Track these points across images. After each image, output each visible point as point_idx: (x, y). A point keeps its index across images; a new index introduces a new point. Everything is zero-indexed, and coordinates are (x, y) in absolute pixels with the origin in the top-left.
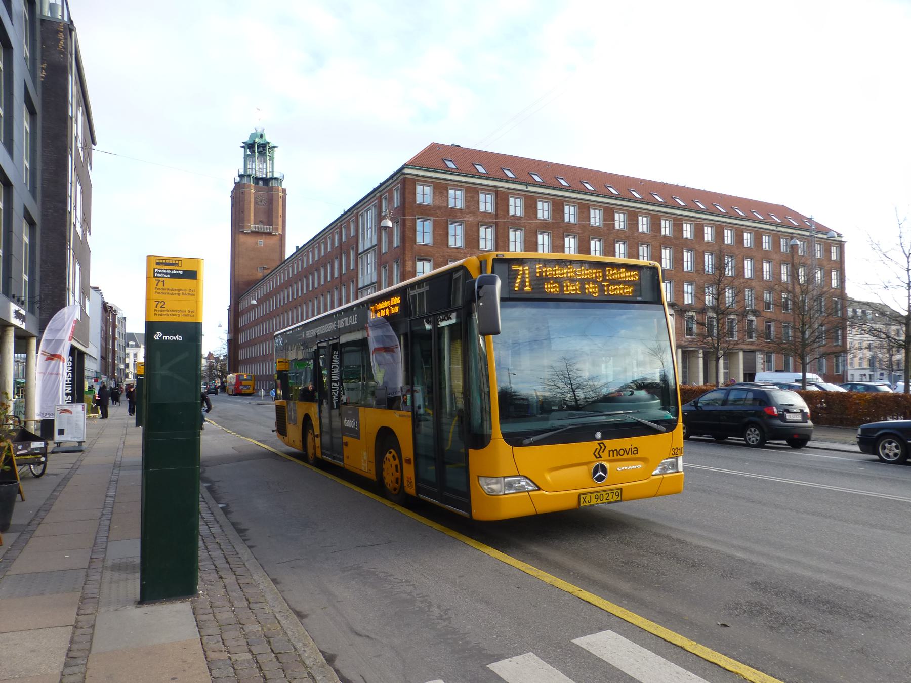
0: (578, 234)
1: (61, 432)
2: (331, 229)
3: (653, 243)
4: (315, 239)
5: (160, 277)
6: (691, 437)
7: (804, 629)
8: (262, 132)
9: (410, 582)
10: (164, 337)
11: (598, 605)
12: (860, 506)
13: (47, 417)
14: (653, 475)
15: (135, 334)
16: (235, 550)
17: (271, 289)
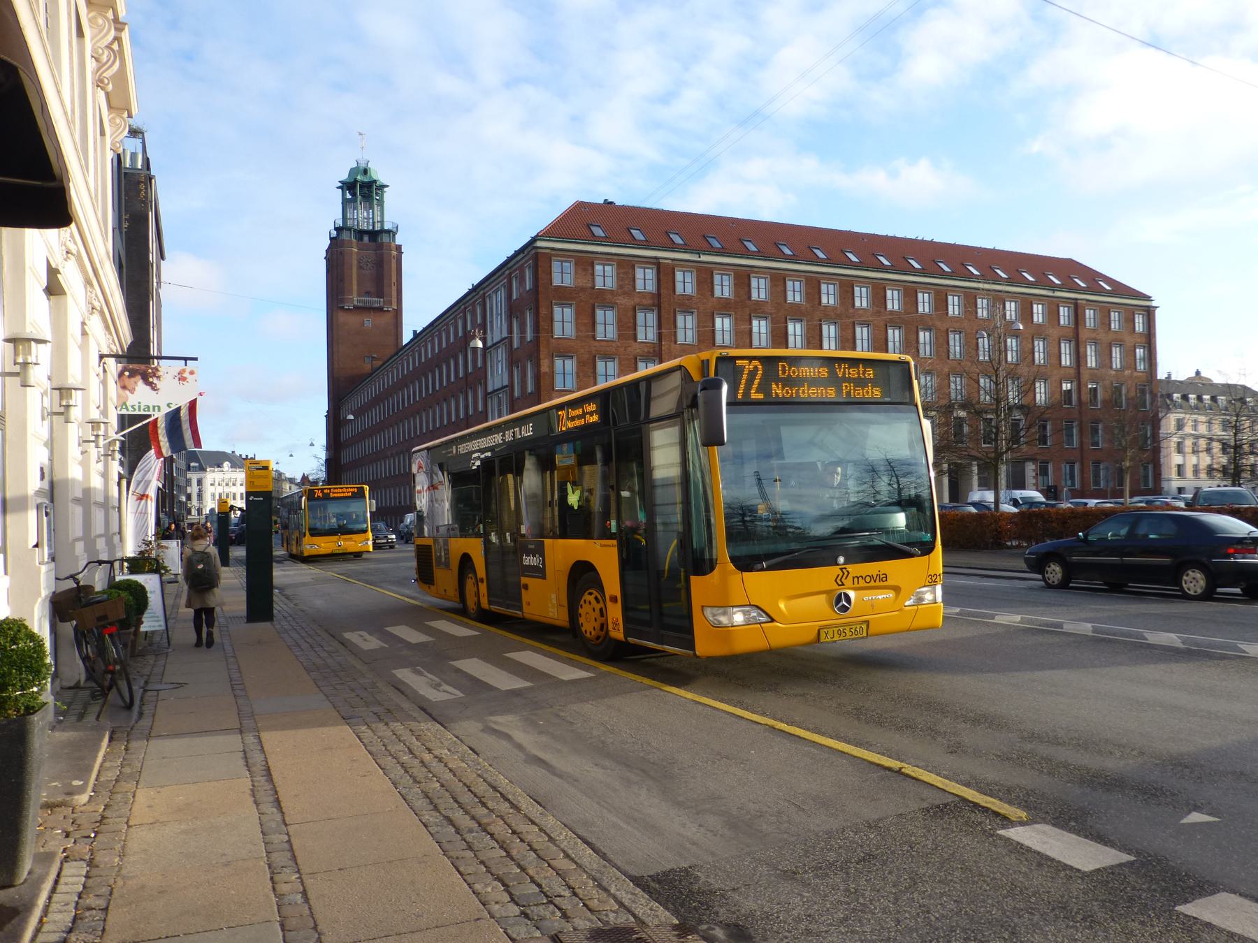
3: (876, 322)
4: (435, 325)
17: (452, 340)
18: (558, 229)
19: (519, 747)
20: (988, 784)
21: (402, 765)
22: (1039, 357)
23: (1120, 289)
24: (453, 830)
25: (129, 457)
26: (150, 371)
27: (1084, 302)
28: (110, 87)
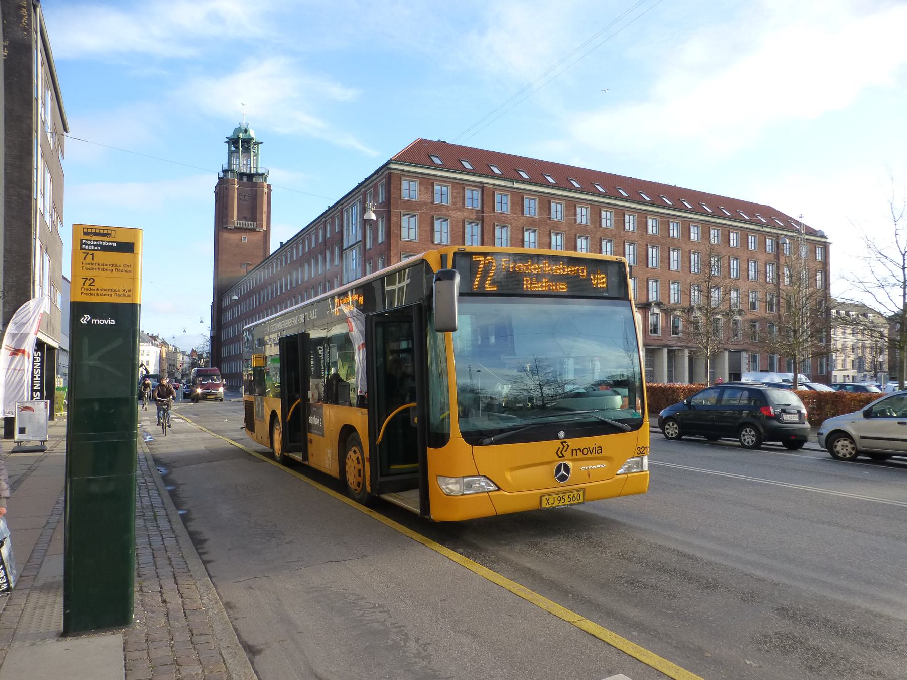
0: (565, 231)
1: (22, 431)
2: (315, 225)
4: (300, 235)
5: (88, 250)
6: (683, 437)
7: (850, 670)
8: (246, 127)
9: (384, 607)
10: (93, 320)
11: (605, 639)
12: (878, 515)
13: (9, 415)
14: (617, 475)
16: (187, 567)
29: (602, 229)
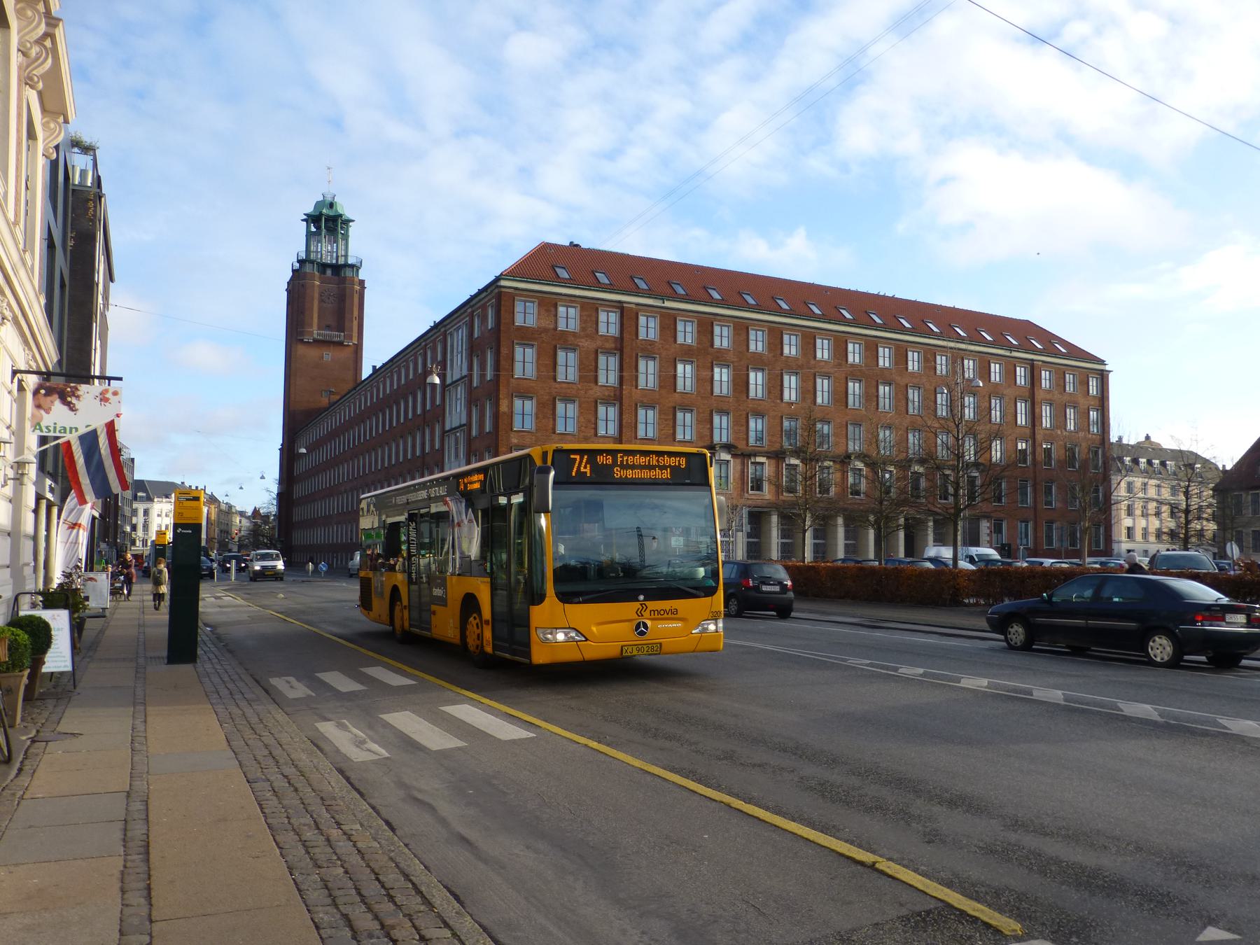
3: (836, 374)
4: (395, 361)
15: (147, 481)
18: (525, 268)
19: (443, 821)
20: (973, 885)
21: (304, 843)
22: (996, 415)
23: (1076, 352)
24: (349, 934)
25: (62, 485)
26: (69, 389)
27: (1040, 363)
28: (40, 85)
29: (783, 358)
